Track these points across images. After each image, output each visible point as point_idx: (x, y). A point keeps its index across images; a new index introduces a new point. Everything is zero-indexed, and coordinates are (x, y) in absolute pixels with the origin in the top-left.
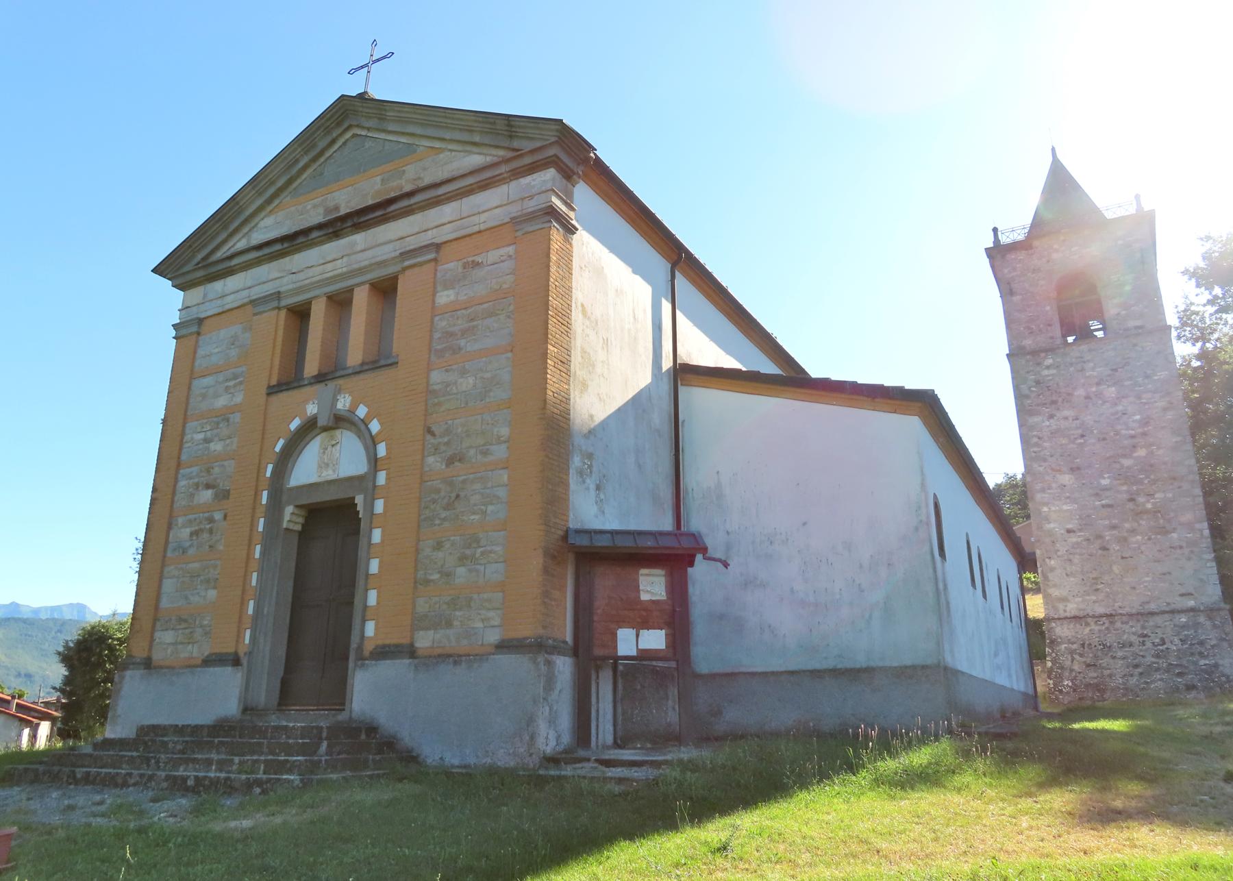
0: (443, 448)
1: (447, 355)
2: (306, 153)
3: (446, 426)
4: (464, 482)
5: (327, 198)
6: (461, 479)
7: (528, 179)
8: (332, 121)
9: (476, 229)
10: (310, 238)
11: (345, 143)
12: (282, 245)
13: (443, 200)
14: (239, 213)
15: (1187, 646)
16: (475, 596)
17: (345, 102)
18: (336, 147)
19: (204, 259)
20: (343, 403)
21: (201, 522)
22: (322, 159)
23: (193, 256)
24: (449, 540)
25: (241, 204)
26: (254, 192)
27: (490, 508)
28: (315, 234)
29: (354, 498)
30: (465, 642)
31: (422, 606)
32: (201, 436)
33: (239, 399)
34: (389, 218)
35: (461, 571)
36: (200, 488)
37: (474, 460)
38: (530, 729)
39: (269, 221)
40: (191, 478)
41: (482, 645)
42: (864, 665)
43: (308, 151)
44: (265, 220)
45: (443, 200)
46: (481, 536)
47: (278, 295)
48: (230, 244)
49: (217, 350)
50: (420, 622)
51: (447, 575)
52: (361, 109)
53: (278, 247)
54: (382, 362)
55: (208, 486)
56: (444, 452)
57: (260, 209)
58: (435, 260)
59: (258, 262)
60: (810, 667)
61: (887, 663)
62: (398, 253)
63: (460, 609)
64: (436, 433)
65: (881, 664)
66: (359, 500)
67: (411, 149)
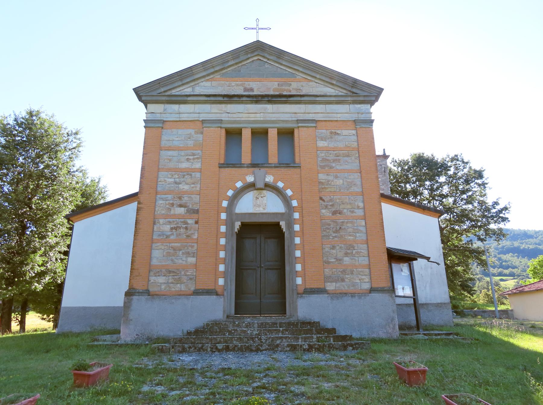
0: (329, 207)
1: (326, 168)
2: (233, 59)
3: (330, 198)
4: (343, 222)
5: (245, 83)
6: (341, 221)
7: (359, 106)
8: (250, 49)
9: (336, 119)
10: (241, 100)
11: (253, 61)
12: (224, 98)
13: (317, 103)
14: (193, 74)
16: (355, 270)
17: (259, 44)
18: (248, 61)
19: (165, 92)
20: (269, 179)
21: (178, 223)
22: (240, 65)
23: (159, 88)
24: (339, 246)
25: (193, 71)
26: (202, 68)
27: (358, 235)
28: (244, 99)
29: (279, 222)
30: (352, 288)
31: (327, 271)
32: (172, 180)
33: (198, 165)
34: (288, 103)
35: (346, 259)
36: (175, 206)
37: (346, 214)
38: (393, 322)
40: (166, 200)
41: (361, 289)
42: (425, 302)
43: (235, 58)
44: (204, 83)
45: (317, 103)
46: (355, 245)
47: (221, 121)
48: (181, 88)
49: (177, 139)
50: (327, 279)
52: (268, 50)
53: (221, 99)
54: (292, 165)
55: (181, 206)
56: (331, 208)
57: (204, 77)
58: (316, 127)
60: (405, 303)
61: (432, 302)
62: (296, 119)
63: (348, 275)
64: (325, 200)
65: (430, 302)
66: (283, 224)
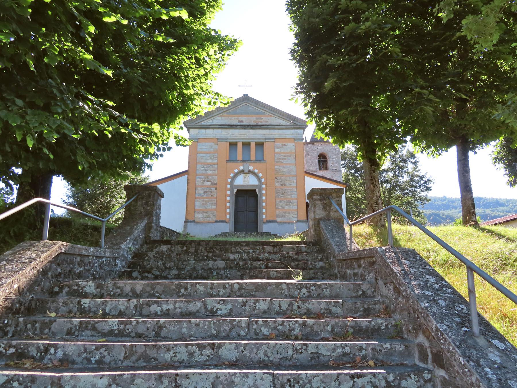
15: (439, 335)
20: (251, 168)
28: (238, 127)
39: (220, 118)
47: (227, 139)
50: (277, 216)
51: (283, 207)
53: (227, 127)
55: (208, 181)
59: (219, 128)
67: (263, 113)
